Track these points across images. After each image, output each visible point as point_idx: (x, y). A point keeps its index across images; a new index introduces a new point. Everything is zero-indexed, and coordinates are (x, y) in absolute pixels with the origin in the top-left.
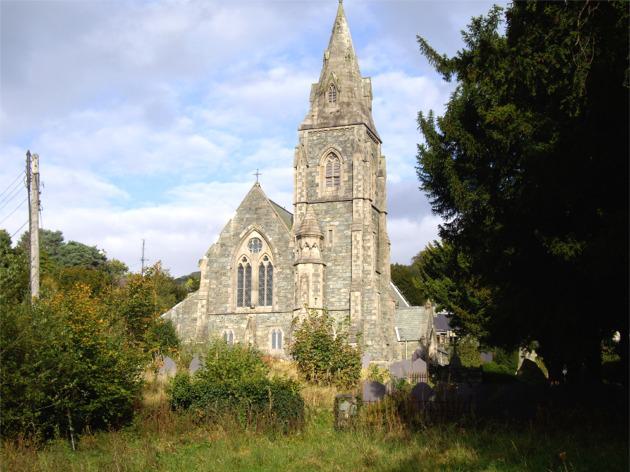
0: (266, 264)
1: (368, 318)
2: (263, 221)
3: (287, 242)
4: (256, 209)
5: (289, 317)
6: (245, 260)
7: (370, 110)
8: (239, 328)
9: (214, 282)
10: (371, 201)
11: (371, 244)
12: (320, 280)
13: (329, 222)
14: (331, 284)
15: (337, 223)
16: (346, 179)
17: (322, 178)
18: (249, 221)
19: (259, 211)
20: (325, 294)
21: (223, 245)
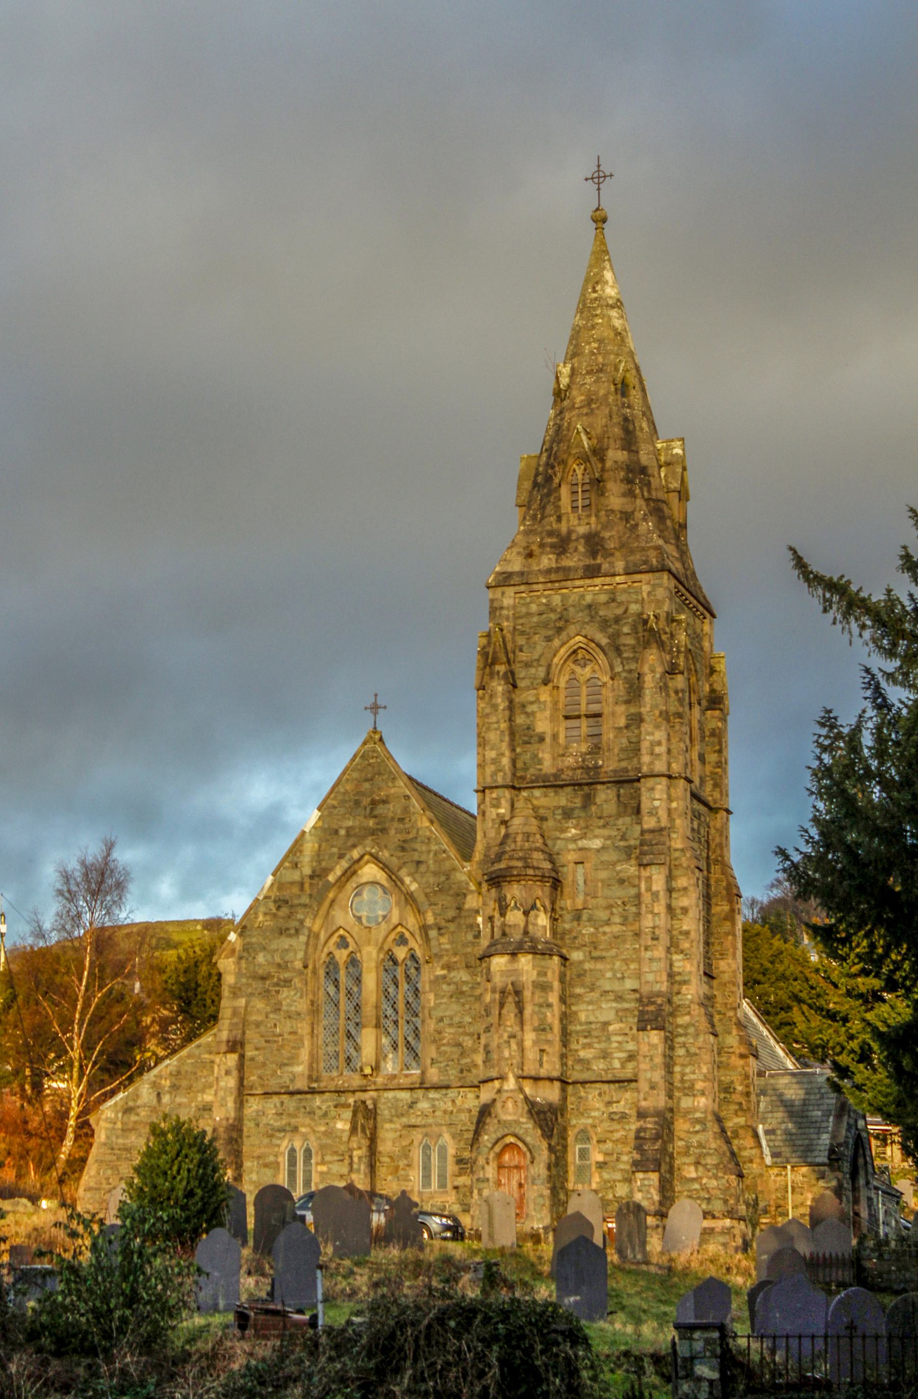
0: (401, 953)
1: (686, 1103)
2: (394, 836)
3: (461, 895)
4: (374, 803)
5: (471, 1101)
6: (343, 943)
7: (683, 495)
8: (329, 1133)
9: (259, 1004)
10: (690, 781)
11: (690, 900)
12: (553, 998)
13: (574, 840)
14: (584, 1013)
15: (597, 843)
16: (622, 722)
17: (552, 719)
18: (355, 837)
19: (380, 810)
20: (565, 1036)
21: (280, 903)
